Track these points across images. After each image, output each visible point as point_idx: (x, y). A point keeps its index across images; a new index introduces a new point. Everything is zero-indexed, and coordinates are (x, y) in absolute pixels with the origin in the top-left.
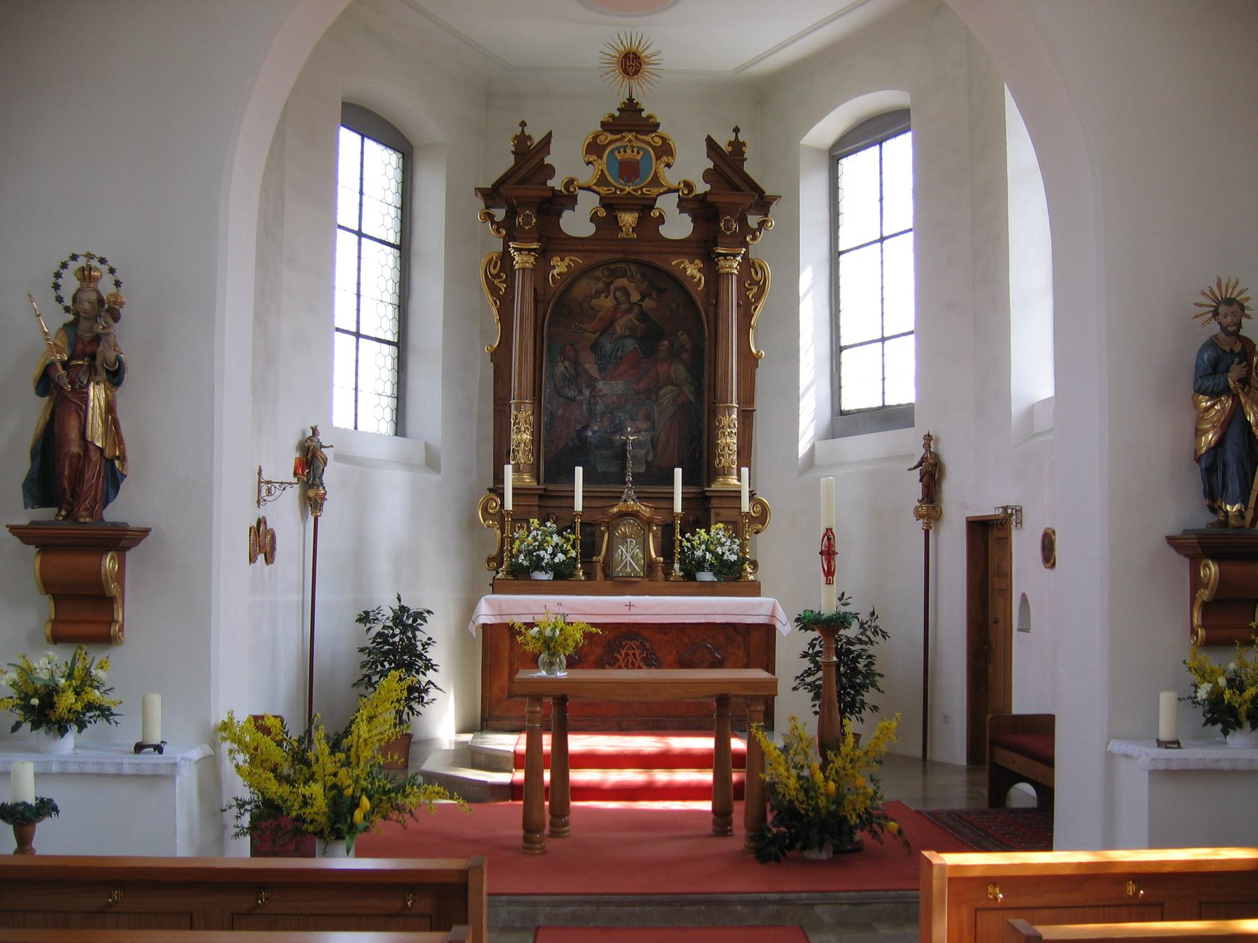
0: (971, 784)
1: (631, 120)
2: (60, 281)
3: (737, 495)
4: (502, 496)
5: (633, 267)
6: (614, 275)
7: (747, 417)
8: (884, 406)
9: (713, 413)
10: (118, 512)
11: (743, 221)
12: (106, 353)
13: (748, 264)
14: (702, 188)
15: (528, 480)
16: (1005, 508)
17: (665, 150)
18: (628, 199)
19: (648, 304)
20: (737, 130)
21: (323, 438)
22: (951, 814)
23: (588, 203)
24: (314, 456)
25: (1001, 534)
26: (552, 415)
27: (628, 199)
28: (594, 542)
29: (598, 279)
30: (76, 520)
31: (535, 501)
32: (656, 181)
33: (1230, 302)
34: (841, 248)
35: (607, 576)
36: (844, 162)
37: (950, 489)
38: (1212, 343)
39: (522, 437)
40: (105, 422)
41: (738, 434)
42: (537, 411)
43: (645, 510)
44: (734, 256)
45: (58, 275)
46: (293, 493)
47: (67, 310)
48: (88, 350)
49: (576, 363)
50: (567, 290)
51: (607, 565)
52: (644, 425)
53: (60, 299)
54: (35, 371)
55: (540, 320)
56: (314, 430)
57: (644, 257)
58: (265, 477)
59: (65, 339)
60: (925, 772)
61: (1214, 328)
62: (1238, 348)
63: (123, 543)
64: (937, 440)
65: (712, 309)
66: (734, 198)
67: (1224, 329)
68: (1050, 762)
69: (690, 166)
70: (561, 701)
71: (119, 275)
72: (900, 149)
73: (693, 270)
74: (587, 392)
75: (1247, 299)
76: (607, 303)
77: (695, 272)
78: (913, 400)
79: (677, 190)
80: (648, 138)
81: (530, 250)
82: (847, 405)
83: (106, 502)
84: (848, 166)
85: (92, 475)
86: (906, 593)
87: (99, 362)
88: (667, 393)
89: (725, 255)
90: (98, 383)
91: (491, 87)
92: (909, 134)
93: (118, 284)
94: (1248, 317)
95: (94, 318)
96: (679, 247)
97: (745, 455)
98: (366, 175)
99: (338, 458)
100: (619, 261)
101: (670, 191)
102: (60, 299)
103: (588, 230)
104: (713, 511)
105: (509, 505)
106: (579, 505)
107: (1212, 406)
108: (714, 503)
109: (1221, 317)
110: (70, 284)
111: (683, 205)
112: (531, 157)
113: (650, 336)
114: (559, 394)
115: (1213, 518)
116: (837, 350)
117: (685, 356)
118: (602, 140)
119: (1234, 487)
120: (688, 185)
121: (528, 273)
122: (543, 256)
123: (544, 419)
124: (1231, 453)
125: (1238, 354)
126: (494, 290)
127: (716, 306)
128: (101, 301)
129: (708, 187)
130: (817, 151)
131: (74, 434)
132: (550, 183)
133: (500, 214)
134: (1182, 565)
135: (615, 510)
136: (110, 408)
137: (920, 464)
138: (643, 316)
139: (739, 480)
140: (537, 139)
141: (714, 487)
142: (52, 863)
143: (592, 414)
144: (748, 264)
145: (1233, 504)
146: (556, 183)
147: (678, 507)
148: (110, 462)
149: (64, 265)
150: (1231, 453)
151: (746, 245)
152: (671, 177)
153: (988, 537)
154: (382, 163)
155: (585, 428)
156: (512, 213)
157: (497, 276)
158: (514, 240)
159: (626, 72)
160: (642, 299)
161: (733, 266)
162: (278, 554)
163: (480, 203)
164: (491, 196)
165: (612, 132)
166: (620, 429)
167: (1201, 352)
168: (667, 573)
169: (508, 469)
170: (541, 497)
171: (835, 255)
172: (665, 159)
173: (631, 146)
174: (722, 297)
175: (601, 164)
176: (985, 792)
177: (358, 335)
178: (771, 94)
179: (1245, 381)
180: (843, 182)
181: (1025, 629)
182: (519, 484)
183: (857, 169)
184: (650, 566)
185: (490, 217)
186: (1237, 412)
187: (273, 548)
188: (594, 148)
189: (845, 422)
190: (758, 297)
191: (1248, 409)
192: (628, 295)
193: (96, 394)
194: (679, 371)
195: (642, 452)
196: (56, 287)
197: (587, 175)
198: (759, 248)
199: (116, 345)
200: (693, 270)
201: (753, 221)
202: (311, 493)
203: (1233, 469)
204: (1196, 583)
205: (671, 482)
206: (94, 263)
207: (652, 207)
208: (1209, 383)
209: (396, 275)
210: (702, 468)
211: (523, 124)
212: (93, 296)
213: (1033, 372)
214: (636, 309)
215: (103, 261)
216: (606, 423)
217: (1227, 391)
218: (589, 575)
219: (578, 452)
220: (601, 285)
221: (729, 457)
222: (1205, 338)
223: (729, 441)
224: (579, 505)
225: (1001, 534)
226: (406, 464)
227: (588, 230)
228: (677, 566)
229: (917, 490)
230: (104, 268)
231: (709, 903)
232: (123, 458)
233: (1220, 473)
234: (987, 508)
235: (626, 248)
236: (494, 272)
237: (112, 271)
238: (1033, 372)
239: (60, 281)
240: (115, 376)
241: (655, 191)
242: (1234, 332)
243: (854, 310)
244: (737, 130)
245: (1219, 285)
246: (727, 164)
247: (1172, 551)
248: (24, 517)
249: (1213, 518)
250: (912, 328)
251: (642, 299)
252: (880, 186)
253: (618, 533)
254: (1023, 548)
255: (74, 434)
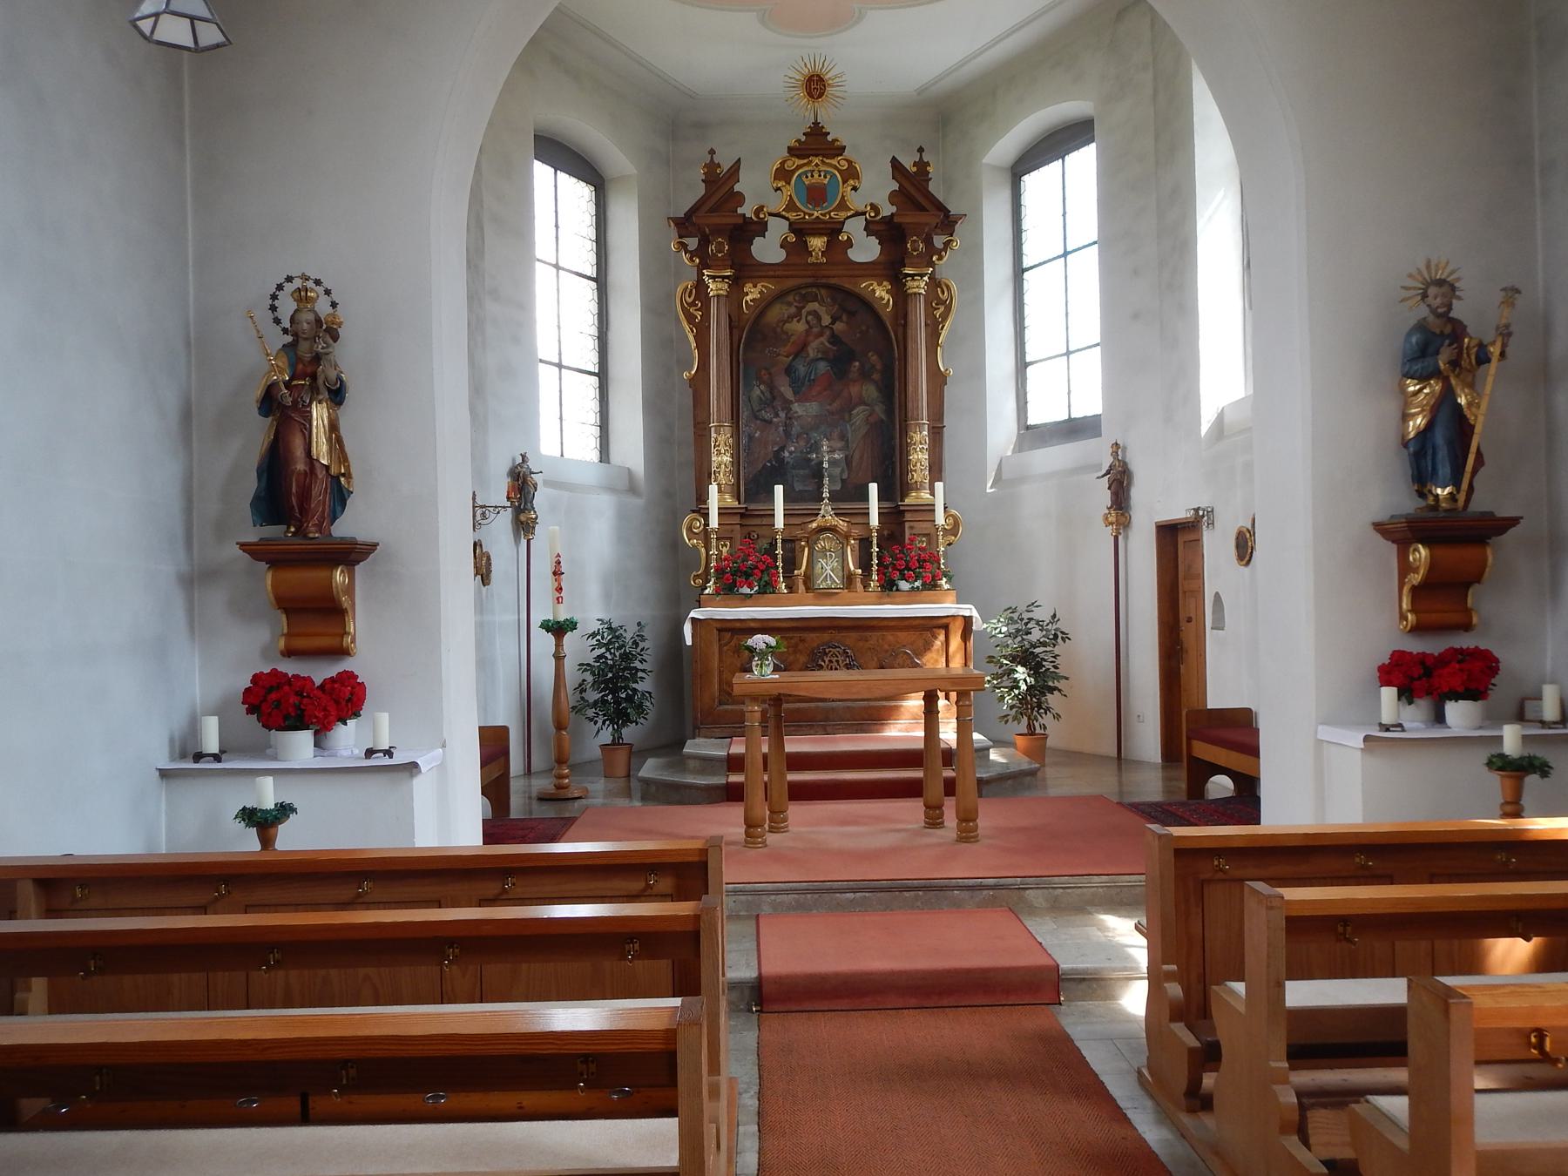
0: (1166, 779)
1: (816, 143)
2: (276, 303)
3: (930, 509)
4: (706, 516)
5: (823, 291)
6: (806, 299)
7: (937, 433)
8: (1070, 420)
9: (904, 432)
10: (347, 527)
11: (928, 241)
12: (326, 372)
13: (935, 283)
14: (887, 210)
15: (730, 501)
16: (1197, 510)
17: (851, 173)
18: (816, 226)
19: (839, 326)
20: (921, 150)
21: (532, 464)
22: (1151, 805)
23: (778, 230)
24: (525, 482)
25: (1192, 537)
26: (751, 438)
27: (816, 226)
28: (794, 558)
29: (790, 304)
30: (305, 536)
31: (737, 520)
32: (843, 205)
33: (1441, 283)
34: (1026, 263)
35: (808, 589)
36: (1026, 178)
37: (1137, 495)
38: (1421, 327)
39: (721, 458)
40: (329, 440)
41: (929, 450)
42: (736, 434)
43: (842, 524)
44: (922, 276)
45: (274, 297)
46: (507, 515)
47: (285, 331)
48: (309, 370)
49: (772, 388)
50: (762, 314)
51: (808, 580)
52: (839, 444)
53: (277, 321)
54: (258, 392)
55: (736, 338)
56: (523, 456)
57: (833, 281)
58: (479, 502)
59: (285, 359)
60: (1120, 769)
61: (1423, 311)
62: (1448, 330)
63: (353, 556)
64: (1125, 449)
65: (900, 330)
66: (922, 218)
67: (1433, 311)
68: (1254, 751)
69: (875, 189)
70: (777, 700)
71: (335, 297)
72: (1084, 162)
73: (881, 292)
74: (782, 415)
75: (1458, 279)
76: (799, 327)
77: (884, 294)
78: (1099, 411)
79: (864, 213)
80: (834, 162)
81: (724, 277)
82: (1032, 420)
83: (334, 519)
84: (1031, 182)
85: (319, 491)
86: (1095, 599)
87: (320, 381)
88: (859, 413)
89: (912, 276)
90: (320, 402)
91: (675, 119)
92: (1093, 145)
93: (334, 305)
94: (1459, 298)
95: (314, 339)
96: (868, 270)
97: (936, 470)
98: (560, 205)
99: (547, 483)
100: (812, 285)
101: (857, 214)
102: (277, 321)
103: (778, 256)
104: (907, 525)
105: (714, 522)
106: (779, 522)
107: (1420, 390)
108: (908, 516)
109: (1430, 300)
110: (287, 306)
111: (870, 229)
112: (721, 182)
113: (841, 358)
114: (756, 418)
115: (1421, 503)
116: (1022, 365)
117: (876, 376)
118: (789, 165)
119: (1444, 470)
120: (874, 207)
121: (723, 300)
122: (736, 283)
123: (744, 441)
124: (1440, 438)
125: (1448, 336)
126: (690, 318)
127: (905, 326)
128: (318, 321)
129: (894, 209)
130: (995, 168)
131: (299, 452)
132: (740, 211)
133: (693, 243)
134: (1391, 550)
135: (814, 525)
136: (333, 427)
137: (1108, 472)
138: (835, 339)
139: (933, 494)
140: (726, 167)
141: (907, 501)
142: (300, 862)
143: (787, 433)
144: (935, 283)
145: (1444, 487)
146: (747, 210)
147: (874, 521)
148: (336, 479)
149: (280, 287)
150: (1440, 438)
151: (932, 264)
152: (857, 201)
153: (1177, 540)
154: (576, 195)
155: (782, 449)
156: (704, 242)
157: (693, 304)
158: (708, 268)
159: (810, 95)
160: (833, 323)
161: (919, 286)
162: (494, 575)
163: (673, 231)
164: (684, 225)
165: (799, 157)
166: (816, 447)
167: (1409, 334)
168: (866, 586)
169: (713, 488)
170: (742, 516)
171: (1019, 271)
172: (851, 182)
173: (818, 171)
174: (911, 317)
175: (789, 191)
176: (1184, 786)
177: (560, 366)
178: (949, 113)
179: (1455, 364)
180: (1027, 199)
181: (1219, 625)
182: (723, 505)
183: (1039, 184)
184: (849, 580)
185: (684, 246)
186: (1448, 395)
187: (489, 571)
188: (783, 174)
189: (1032, 435)
190: (945, 316)
191: (1458, 391)
192: (819, 318)
193: (319, 414)
194: (870, 391)
195: (837, 471)
196: (273, 308)
197: (777, 203)
198: (945, 266)
199: (336, 366)
200: (881, 292)
201: (939, 241)
202: (522, 518)
203: (1443, 453)
204: (1405, 568)
205: (866, 498)
206: (310, 284)
207: (840, 231)
208: (1417, 367)
209: (594, 307)
210: (895, 485)
211: (712, 152)
212: (311, 317)
213: (1223, 374)
214: (828, 333)
215: (318, 282)
216: (802, 443)
217: (1436, 374)
218: (791, 588)
219: (776, 471)
220: (793, 310)
221: (920, 473)
222: (1413, 322)
223: (920, 457)
224: (779, 522)
225: (1192, 537)
226: (611, 489)
227: (778, 256)
228: (875, 577)
229: (1105, 497)
230: (320, 290)
231: (926, 888)
232: (348, 475)
233: (1429, 458)
234: (1178, 512)
235: (818, 277)
236: (690, 300)
237: (328, 292)
238: (1223, 374)
239: (276, 303)
240: (337, 395)
241: (843, 215)
242: (1445, 316)
243: (1042, 322)
244: (921, 150)
245: (1428, 267)
246: (913, 186)
247: (1378, 539)
248: (253, 535)
249: (1421, 503)
250: (1098, 340)
251: (833, 323)
252: (1065, 199)
253: (818, 547)
254: (1216, 548)
255: (299, 452)
